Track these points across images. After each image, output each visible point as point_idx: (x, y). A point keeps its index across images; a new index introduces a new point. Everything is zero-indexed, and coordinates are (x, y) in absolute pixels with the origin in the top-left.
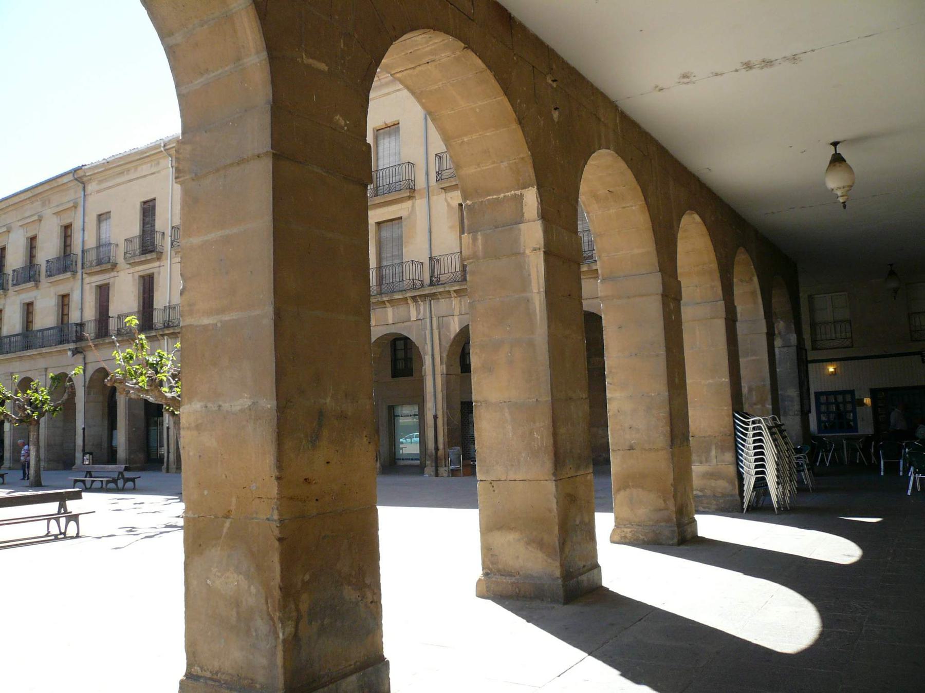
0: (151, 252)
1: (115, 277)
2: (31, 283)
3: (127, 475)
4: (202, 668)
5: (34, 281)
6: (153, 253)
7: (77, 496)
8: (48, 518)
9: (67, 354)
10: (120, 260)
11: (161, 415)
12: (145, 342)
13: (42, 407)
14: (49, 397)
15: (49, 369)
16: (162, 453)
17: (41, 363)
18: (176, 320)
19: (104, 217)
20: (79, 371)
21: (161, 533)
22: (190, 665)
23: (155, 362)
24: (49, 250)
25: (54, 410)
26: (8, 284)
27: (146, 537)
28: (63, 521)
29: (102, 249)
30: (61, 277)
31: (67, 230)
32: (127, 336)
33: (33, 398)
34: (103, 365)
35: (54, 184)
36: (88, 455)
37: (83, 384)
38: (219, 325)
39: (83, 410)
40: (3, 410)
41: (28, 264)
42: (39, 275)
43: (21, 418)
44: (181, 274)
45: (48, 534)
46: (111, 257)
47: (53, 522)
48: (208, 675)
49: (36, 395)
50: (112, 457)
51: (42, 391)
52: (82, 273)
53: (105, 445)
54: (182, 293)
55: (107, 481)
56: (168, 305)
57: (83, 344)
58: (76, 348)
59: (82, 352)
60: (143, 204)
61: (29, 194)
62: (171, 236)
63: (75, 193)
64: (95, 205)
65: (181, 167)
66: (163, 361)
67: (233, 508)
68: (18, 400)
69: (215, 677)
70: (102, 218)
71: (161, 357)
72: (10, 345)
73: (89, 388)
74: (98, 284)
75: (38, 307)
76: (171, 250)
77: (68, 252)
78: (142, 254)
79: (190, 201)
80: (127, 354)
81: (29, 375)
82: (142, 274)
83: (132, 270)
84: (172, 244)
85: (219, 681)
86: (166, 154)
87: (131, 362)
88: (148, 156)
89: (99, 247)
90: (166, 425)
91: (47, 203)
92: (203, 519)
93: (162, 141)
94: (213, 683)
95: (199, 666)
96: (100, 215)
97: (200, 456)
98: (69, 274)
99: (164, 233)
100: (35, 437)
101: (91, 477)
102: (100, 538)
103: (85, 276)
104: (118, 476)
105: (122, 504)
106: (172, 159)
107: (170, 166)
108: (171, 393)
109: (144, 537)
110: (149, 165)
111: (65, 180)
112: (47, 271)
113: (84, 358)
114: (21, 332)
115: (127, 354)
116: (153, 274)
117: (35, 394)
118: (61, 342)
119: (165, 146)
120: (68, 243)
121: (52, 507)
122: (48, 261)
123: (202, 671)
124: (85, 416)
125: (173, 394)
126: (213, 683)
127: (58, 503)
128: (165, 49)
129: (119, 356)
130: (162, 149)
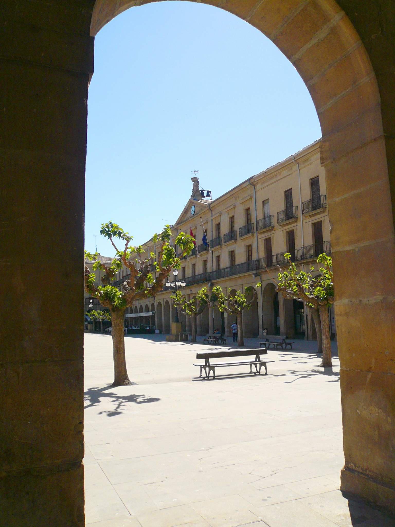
0: (292, 218)
1: (273, 233)
2: (232, 241)
3: (287, 341)
4: (355, 465)
5: (234, 239)
6: (293, 219)
7: (265, 352)
8: (251, 363)
9: (252, 276)
10: (276, 224)
11: (303, 308)
12: (295, 267)
13: (242, 305)
14: (245, 299)
15: (244, 285)
16: (304, 329)
17: (240, 282)
18: (308, 255)
19: (266, 202)
20: (259, 285)
21: (310, 375)
22: (347, 462)
23: (300, 278)
24: (240, 223)
25: (249, 306)
26: (222, 242)
27: (302, 377)
28: (258, 365)
29: (266, 219)
30: (247, 236)
31: (248, 211)
32: (285, 265)
33: (238, 300)
34: (271, 281)
35: (240, 188)
36: (265, 330)
37: (261, 292)
38: (357, 250)
39: (262, 306)
40: (224, 306)
41: (246, 224)
42: (236, 236)
43: (233, 310)
44: (329, 221)
45: (251, 372)
46: (271, 223)
47: (253, 366)
48: (360, 470)
49: (239, 298)
50: (277, 331)
51: (242, 296)
52: (257, 233)
53: (273, 325)
54: (331, 232)
55: (277, 344)
56: (303, 246)
57: (260, 271)
58: (257, 273)
59: (259, 275)
60: (285, 192)
61: (228, 195)
62: (302, 208)
63: (250, 191)
64: (261, 196)
65: (324, 156)
66: (304, 278)
67: (373, 365)
68: (231, 301)
69: (365, 472)
70: (265, 202)
71: (303, 275)
72: (225, 273)
73: (264, 294)
74: (266, 238)
75: (237, 252)
76: (302, 216)
77: (249, 223)
78: (287, 220)
79: (331, 176)
80: (285, 275)
81: (234, 288)
82: (288, 230)
83: (282, 229)
84: (303, 212)
85: (368, 475)
86: (295, 163)
87: (287, 279)
88: (286, 166)
89: (264, 218)
90: (305, 314)
91: (237, 198)
92: (353, 372)
93: (293, 156)
94: (364, 476)
95: (353, 463)
96: (264, 201)
97: (349, 332)
98: (250, 235)
99: (298, 207)
100: (240, 320)
101: (268, 342)
102: (278, 376)
103: (258, 234)
104: (283, 342)
105: (286, 358)
106: (299, 165)
107: (298, 169)
108: (311, 295)
109: (301, 377)
110: (287, 171)
111: (245, 185)
112: (239, 234)
113: (261, 278)
114: (229, 266)
115: (285, 275)
116: (294, 230)
117: (239, 298)
118: (249, 270)
119: (294, 159)
120: (249, 218)
121: (252, 358)
122: (240, 229)
123: (355, 467)
124: (263, 309)
125: (312, 296)
126: (364, 476)
127: (255, 356)
128: (308, 88)
129: (280, 275)
130: (293, 160)
